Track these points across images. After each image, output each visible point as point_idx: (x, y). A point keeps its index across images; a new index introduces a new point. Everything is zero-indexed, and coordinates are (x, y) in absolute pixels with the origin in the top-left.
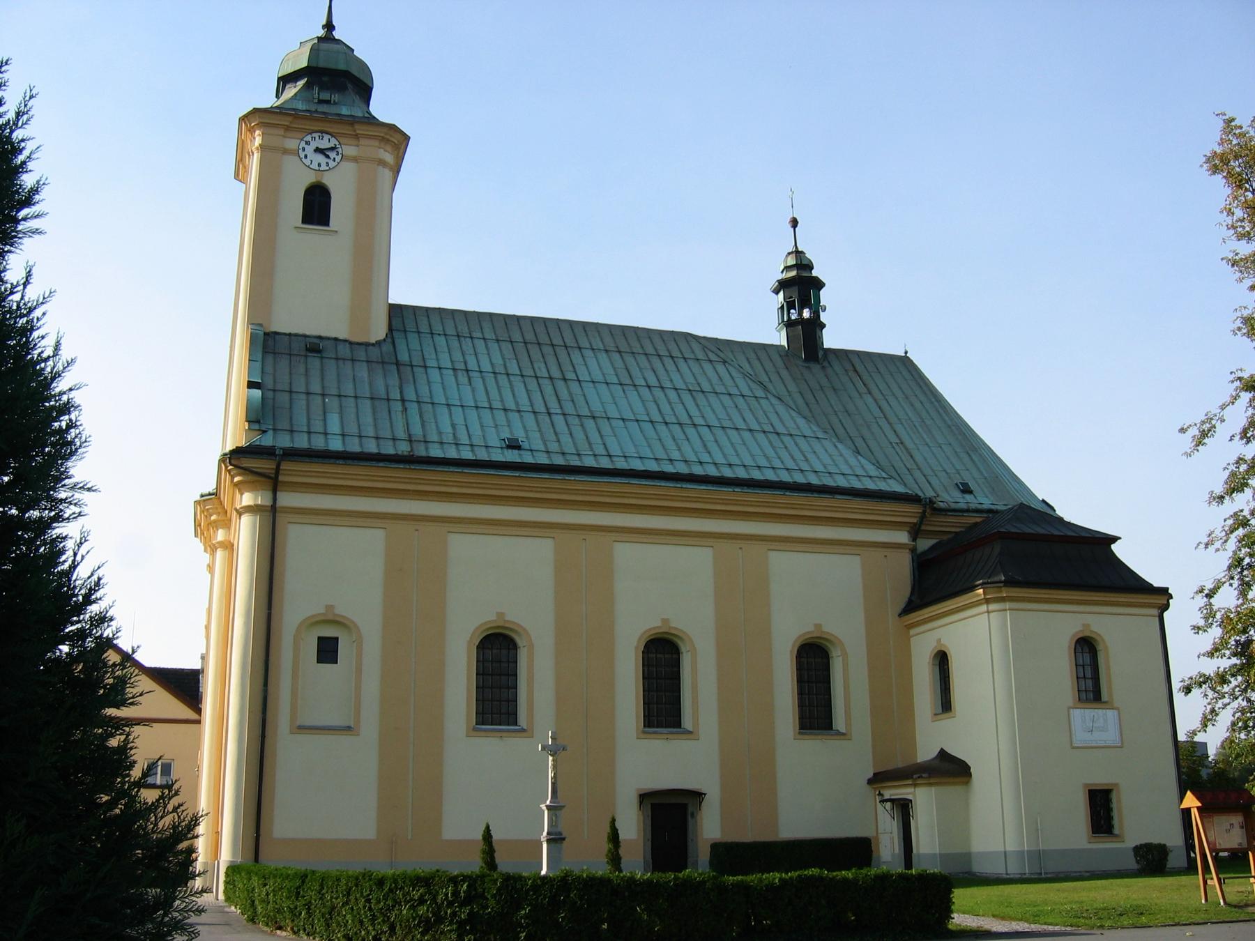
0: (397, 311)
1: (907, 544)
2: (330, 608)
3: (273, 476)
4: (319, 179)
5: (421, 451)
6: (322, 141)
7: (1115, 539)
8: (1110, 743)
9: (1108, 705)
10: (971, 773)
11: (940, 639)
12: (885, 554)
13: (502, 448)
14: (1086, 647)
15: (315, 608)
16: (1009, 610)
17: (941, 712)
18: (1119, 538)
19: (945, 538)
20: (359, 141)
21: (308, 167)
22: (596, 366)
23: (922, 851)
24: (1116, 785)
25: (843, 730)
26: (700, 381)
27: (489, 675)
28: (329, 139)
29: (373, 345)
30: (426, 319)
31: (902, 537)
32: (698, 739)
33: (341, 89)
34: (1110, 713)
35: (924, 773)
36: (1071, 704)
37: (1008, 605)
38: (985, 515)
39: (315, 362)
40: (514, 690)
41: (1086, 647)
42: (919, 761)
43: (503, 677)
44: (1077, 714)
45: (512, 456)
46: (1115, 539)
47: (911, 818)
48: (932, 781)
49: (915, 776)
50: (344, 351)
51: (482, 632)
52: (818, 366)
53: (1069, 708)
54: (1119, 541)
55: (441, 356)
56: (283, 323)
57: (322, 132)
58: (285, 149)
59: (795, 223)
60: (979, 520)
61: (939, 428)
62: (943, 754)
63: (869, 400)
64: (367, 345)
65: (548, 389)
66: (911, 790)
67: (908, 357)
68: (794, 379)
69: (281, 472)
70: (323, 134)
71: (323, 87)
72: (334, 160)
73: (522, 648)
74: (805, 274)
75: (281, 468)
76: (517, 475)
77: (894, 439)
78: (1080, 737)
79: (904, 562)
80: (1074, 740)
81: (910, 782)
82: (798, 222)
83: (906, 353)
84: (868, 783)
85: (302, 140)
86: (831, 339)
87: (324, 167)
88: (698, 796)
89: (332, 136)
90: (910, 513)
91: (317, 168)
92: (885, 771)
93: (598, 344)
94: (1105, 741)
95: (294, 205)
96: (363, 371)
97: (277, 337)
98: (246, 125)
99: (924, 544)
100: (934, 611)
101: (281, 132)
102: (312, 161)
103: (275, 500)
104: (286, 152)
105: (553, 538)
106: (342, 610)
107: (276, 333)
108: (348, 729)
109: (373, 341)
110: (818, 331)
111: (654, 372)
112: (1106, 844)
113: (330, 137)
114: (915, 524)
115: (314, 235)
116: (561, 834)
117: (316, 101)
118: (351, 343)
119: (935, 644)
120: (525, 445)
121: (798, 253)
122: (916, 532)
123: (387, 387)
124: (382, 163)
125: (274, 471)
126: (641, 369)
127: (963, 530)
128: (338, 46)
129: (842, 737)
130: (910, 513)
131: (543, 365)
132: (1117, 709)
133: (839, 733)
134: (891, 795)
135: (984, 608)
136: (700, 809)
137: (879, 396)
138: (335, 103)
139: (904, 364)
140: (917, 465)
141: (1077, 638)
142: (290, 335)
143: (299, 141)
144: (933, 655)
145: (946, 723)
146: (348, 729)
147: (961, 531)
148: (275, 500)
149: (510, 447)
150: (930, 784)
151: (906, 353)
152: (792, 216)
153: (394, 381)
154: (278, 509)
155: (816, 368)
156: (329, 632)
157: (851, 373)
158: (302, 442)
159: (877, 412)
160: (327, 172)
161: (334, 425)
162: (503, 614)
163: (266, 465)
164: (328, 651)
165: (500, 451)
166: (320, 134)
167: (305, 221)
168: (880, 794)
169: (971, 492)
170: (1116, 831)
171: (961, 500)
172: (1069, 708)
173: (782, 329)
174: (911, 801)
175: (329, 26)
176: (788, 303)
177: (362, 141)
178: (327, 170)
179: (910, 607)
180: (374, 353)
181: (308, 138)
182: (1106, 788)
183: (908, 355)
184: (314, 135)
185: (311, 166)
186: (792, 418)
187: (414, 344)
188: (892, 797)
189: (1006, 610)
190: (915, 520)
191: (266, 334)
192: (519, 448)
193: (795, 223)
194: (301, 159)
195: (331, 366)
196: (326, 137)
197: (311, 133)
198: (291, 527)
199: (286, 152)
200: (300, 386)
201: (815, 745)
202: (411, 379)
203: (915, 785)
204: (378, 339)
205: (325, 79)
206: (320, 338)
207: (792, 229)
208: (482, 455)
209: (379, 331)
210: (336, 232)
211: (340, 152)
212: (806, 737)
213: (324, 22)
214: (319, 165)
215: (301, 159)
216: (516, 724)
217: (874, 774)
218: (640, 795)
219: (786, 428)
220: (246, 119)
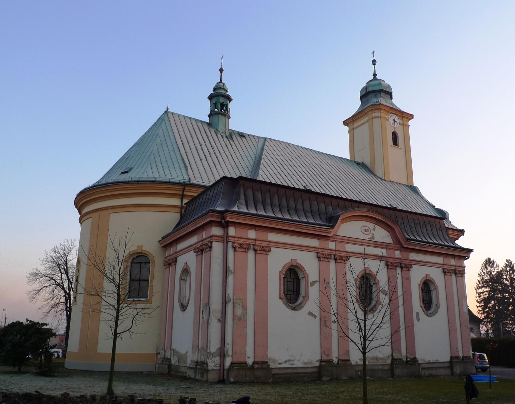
175: (375, 75)
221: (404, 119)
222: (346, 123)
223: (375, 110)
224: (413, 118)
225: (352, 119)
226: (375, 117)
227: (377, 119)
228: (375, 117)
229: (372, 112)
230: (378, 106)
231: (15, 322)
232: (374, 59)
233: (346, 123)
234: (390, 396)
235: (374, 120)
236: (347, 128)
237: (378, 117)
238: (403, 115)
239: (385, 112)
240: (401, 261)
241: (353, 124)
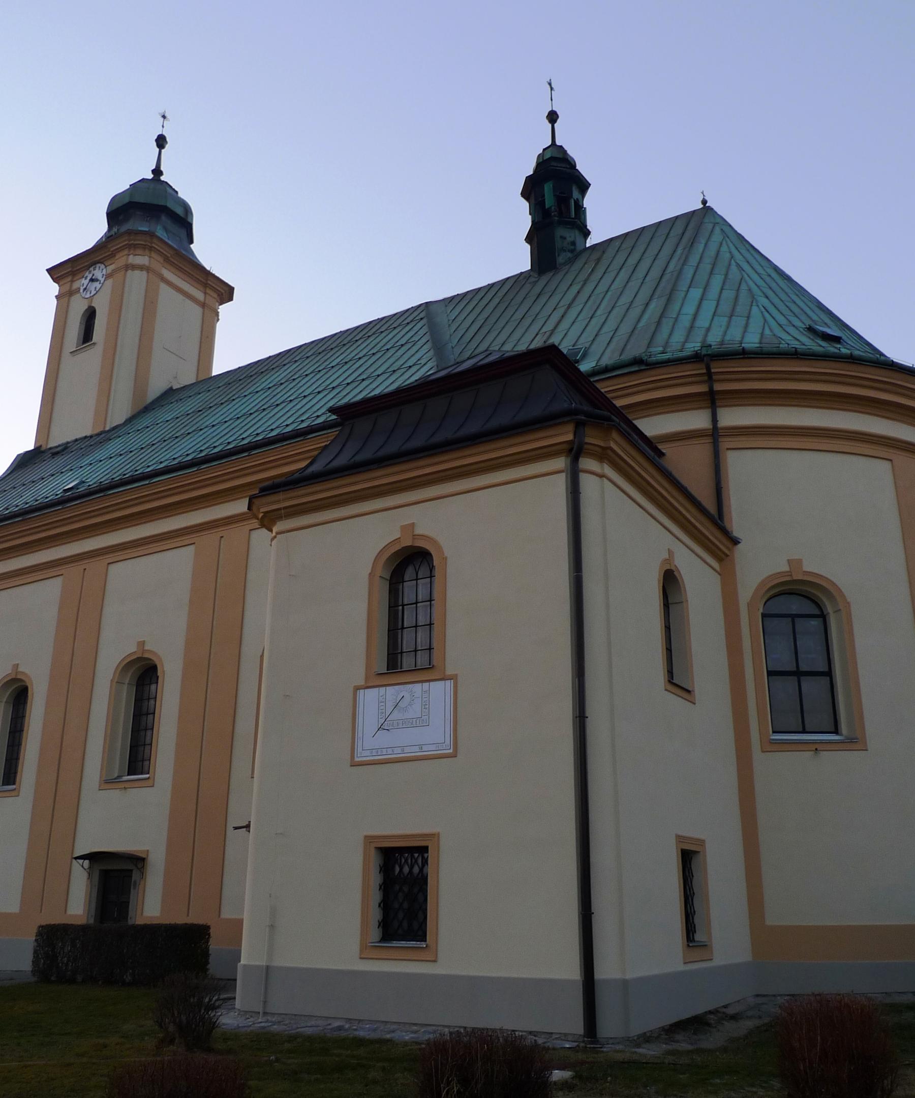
8: (430, 750)
15: (129, 649)
24: (435, 836)
43: (808, 685)
53: (357, 688)
80: (359, 749)
94: (421, 746)
103: (714, 420)
110: (576, 194)
111: (672, 226)
132: (453, 678)
148: (714, 420)
152: (551, 109)
154: (721, 433)
162: (800, 562)
175: (157, 172)
182: (680, 853)
213: (154, 167)
221: (208, 291)
222: (56, 272)
223: (135, 246)
224: (230, 298)
225: (70, 265)
226: (134, 267)
227: (137, 273)
228: (134, 267)
229: (129, 251)
230: (148, 243)
231: (208, 967)
232: (164, 133)
233: (56, 272)
234: (819, 1032)
235: (130, 272)
236: (55, 288)
237: (141, 268)
238: (207, 281)
239: (161, 259)
240: (151, 243)
241: (72, 281)
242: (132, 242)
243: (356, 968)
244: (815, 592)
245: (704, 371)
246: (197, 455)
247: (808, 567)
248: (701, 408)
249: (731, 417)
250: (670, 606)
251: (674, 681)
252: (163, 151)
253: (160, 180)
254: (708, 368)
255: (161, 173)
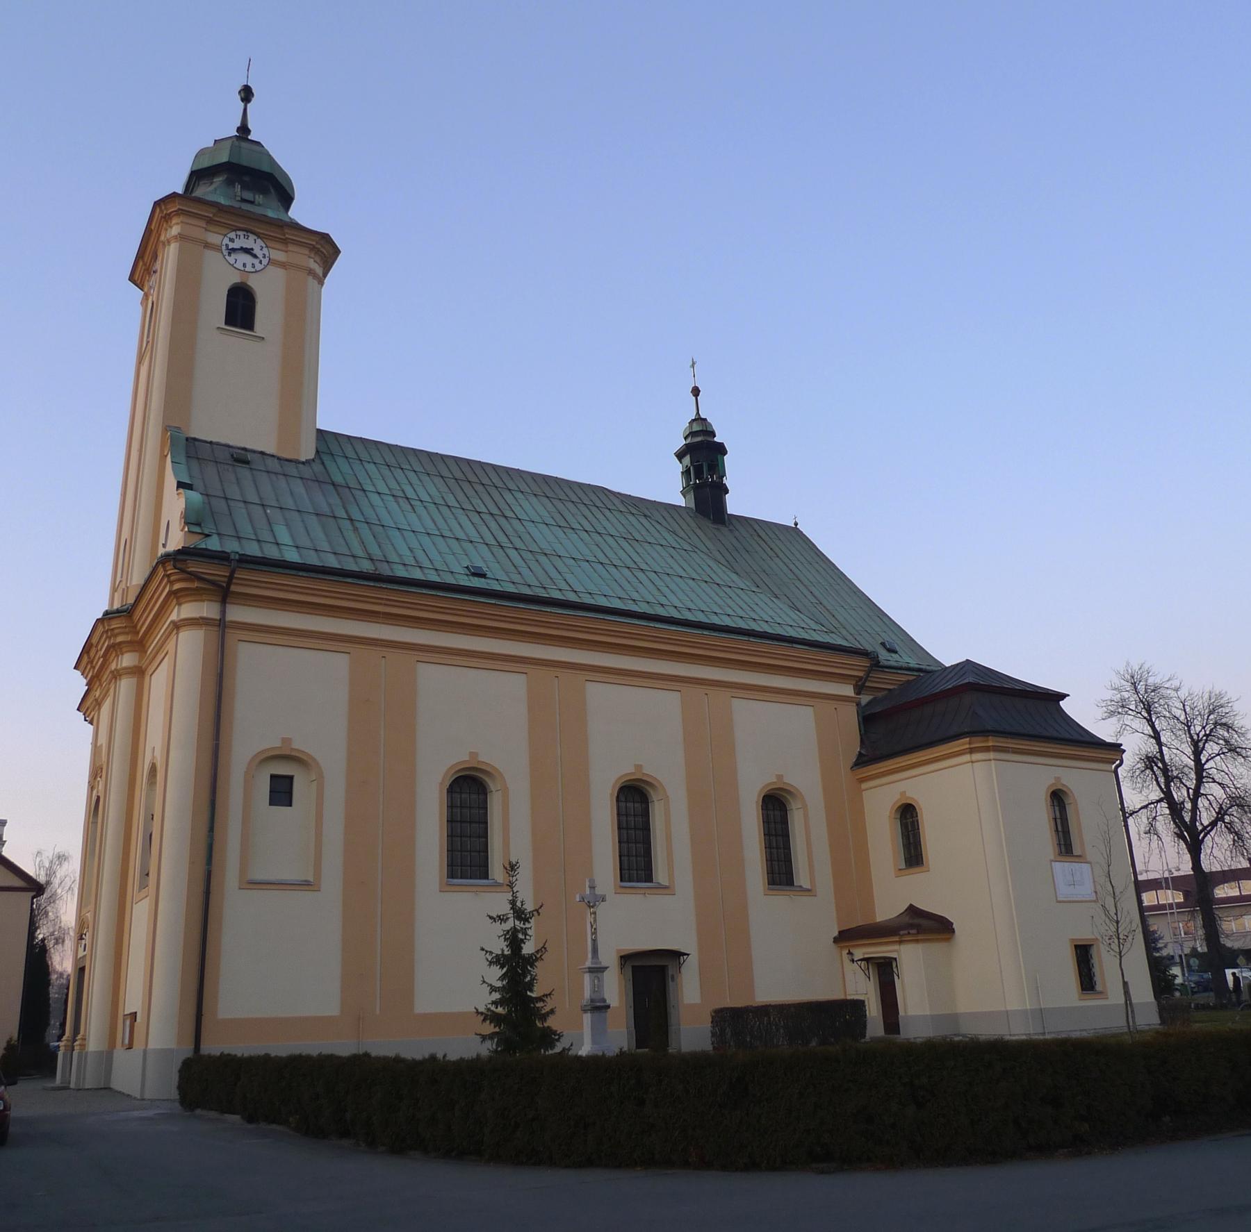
0: (323, 435)
1: (852, 697)
2: (286, 741)
3: (225, 585)
4: (244, 280)
5: (385, 570)
6: (247, 241)
7: (1063, 696)
9: (1081, 858)
10: (954, 929)
11: (905, 792)
12: (836, 707)
13: (467, 575)
14: (1058, 798)
15: (272, 742)
16: (994, 759)
17: (904, 867)
18: (1068, 695)
19: (880, 694)
20: (287, 247)
21: (232, 265)
22: (529, 507)
23: (911, 1012)
25: (806, 885)
26: (631, 531)
27: (457, 821)
28: (255, 240)
29: (303, 463)
30: (350, 446)
31: (848, 690)
32: (674, 894)
33: (264, 192)
34: (1086, 867)
35: (912, 929)
36: (1052, 857)
37: (992, 755)
38: (915, 673)
39: (244, 472)
40: (484, 839)
41: (1058, 798)
42: (878, 920)
44: (1057, 866)
45: (477, 583)
46: (1063, 696)
47: (896, 977)
48: (920, 937)
49: (902, 932)
50: (273, 465)
51: (452, 776)
52: (726, 529)
53: (1052, 861)
54: (1067, 698)
55: (277, 529)
56: (203, 430)
57: (247, 231)
58: (207, 243)
59: (696, 392)
60: (911, 678)
61: (846, 592)
62: (912, 910)
63: (777, 560)
64: (297, 462)
65: (493, 525)
66: (896, 947)
67: (798, 529)
68: (709, 539)
69: (234, 581)
70: (249, 234)
71: (245, 187)
72: (261, 262)
73: (494, 792)
74: (710, 439)
75: (235, 576)
76: (494, 602)
77: (814, 600)
78: (1064, 891)
79: (850, 716)
81: (897, 939)
82: (700, 391)
83: (796, 524)
84: (834, 942)
85: (225, 235)
86: (735, 505)
87: (249, 268)
88: (676, 956)
89: (259, 237)
90: (857, 667)
91: (243, 269)
92: (849, 929)
93: (524, 487)
95: (215, 306)
96: (299, 488)
97: (197, 443)
98: (161, 211)
99: (865, 699)
100: (899, 763)
101: (203, 224)
102: (236, 260)
103: (223, 612)
104: (207, 246)
105: (526, 673)
106: (300, 744)
107: (195, 439)
108: (305, 885)
109: (303, 459)
112: (1091, 1002)
113: (256, 238)
114: (860, 678)
115: (236, 341)
116: (604, 1001)
117: (239, 199)
118: (279, 459)
119: (898, 796)
120: (489, 575)
121: (699, 419)
122: (859, 689)
123: (330, 505)
124: (311, 272)
125: (226, 579)
126: (573, 515)
127: (895, 687)
128: (258, 147)
129: (807, 893)
130: (857, 667)
131: (479, 501)
133: (802, 889)
134: (864, 954)
135: (967, 758)
136: (680, 972)
137: (786, 561)
138: (259, 205)
139: (794, 534)
140: (842, 625)
141: (914, 804)
142: (211, 443)
143: (222, 237)
144: (895, 808)
145: (915, 878)
146: (305, 885)
147: (894, 688)
148: (223, 612)
149: (475, 575)
150: (917, 941)
151: (796, 524)
153: (335, 500)
155: (724, 530)
156: (282, 769)
157: (756, 538)
158: (253, 550)
159: (791, 576)
160: (253, 274)
161: (284, 536)
163: (217, 572)
164: (281, 791)
165: (466, 578)
166: (245, 233)
167: (229, 321)
168: (850, 953)
169: (895, 652)
170: (1099, 987)
171: (890, 658)
172: (1052, 861)
173: (688, 492)
174: (895, 959)
176: (694, 466)
177: (291, 247)
178: (264, 268)
179: (862, 761)
180: (306, 471)
181: (232, 235)
183: (798, 527)
184: (238, 233)
185: (235, 265)
186: (724, 572)
187: (345, 467)
188: (866, 956)
189: (990, 760)
190: (861, 674)
191: (187, 439)
192: (483, 576)
193: (696, 392)
194: (224, 256)
195: (263, 479)
196: (252, 237)
197: (235, 230)
198: (242, 646)
199: (207, 246)
200: (233, 492)
201: (781, 901)
202: (352, 499)
203: (900, 942)
204: (308, 458)
205: (246, 179)
206: (245, 449)
207: (694, 398)
208: (450, 579)
209: (307, 451)
210: (263, 338)
211: (267, 255)
212: (775, 892)
214: (244, 265)
215: (224, 256)
216: (486, 876)
217: (840, 932)
218: (622, 957)
219: (724, 582)
220: (162, 204)
242: (319, 246)
243: (1078, 1005)
244: (477, 774)
245: (228, 574)
246: (93, 671)
247: (296, 745)
248: (212, 601)
249: (237, 613)
250: (1067, 806)
251: (134, 906)
252: (249, 105)
253: (248, 139)
254: (233, 573)
255: (248, 131)
